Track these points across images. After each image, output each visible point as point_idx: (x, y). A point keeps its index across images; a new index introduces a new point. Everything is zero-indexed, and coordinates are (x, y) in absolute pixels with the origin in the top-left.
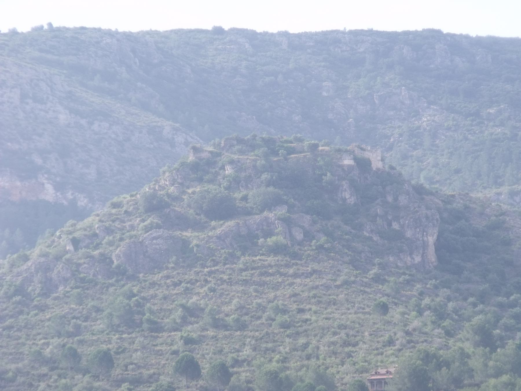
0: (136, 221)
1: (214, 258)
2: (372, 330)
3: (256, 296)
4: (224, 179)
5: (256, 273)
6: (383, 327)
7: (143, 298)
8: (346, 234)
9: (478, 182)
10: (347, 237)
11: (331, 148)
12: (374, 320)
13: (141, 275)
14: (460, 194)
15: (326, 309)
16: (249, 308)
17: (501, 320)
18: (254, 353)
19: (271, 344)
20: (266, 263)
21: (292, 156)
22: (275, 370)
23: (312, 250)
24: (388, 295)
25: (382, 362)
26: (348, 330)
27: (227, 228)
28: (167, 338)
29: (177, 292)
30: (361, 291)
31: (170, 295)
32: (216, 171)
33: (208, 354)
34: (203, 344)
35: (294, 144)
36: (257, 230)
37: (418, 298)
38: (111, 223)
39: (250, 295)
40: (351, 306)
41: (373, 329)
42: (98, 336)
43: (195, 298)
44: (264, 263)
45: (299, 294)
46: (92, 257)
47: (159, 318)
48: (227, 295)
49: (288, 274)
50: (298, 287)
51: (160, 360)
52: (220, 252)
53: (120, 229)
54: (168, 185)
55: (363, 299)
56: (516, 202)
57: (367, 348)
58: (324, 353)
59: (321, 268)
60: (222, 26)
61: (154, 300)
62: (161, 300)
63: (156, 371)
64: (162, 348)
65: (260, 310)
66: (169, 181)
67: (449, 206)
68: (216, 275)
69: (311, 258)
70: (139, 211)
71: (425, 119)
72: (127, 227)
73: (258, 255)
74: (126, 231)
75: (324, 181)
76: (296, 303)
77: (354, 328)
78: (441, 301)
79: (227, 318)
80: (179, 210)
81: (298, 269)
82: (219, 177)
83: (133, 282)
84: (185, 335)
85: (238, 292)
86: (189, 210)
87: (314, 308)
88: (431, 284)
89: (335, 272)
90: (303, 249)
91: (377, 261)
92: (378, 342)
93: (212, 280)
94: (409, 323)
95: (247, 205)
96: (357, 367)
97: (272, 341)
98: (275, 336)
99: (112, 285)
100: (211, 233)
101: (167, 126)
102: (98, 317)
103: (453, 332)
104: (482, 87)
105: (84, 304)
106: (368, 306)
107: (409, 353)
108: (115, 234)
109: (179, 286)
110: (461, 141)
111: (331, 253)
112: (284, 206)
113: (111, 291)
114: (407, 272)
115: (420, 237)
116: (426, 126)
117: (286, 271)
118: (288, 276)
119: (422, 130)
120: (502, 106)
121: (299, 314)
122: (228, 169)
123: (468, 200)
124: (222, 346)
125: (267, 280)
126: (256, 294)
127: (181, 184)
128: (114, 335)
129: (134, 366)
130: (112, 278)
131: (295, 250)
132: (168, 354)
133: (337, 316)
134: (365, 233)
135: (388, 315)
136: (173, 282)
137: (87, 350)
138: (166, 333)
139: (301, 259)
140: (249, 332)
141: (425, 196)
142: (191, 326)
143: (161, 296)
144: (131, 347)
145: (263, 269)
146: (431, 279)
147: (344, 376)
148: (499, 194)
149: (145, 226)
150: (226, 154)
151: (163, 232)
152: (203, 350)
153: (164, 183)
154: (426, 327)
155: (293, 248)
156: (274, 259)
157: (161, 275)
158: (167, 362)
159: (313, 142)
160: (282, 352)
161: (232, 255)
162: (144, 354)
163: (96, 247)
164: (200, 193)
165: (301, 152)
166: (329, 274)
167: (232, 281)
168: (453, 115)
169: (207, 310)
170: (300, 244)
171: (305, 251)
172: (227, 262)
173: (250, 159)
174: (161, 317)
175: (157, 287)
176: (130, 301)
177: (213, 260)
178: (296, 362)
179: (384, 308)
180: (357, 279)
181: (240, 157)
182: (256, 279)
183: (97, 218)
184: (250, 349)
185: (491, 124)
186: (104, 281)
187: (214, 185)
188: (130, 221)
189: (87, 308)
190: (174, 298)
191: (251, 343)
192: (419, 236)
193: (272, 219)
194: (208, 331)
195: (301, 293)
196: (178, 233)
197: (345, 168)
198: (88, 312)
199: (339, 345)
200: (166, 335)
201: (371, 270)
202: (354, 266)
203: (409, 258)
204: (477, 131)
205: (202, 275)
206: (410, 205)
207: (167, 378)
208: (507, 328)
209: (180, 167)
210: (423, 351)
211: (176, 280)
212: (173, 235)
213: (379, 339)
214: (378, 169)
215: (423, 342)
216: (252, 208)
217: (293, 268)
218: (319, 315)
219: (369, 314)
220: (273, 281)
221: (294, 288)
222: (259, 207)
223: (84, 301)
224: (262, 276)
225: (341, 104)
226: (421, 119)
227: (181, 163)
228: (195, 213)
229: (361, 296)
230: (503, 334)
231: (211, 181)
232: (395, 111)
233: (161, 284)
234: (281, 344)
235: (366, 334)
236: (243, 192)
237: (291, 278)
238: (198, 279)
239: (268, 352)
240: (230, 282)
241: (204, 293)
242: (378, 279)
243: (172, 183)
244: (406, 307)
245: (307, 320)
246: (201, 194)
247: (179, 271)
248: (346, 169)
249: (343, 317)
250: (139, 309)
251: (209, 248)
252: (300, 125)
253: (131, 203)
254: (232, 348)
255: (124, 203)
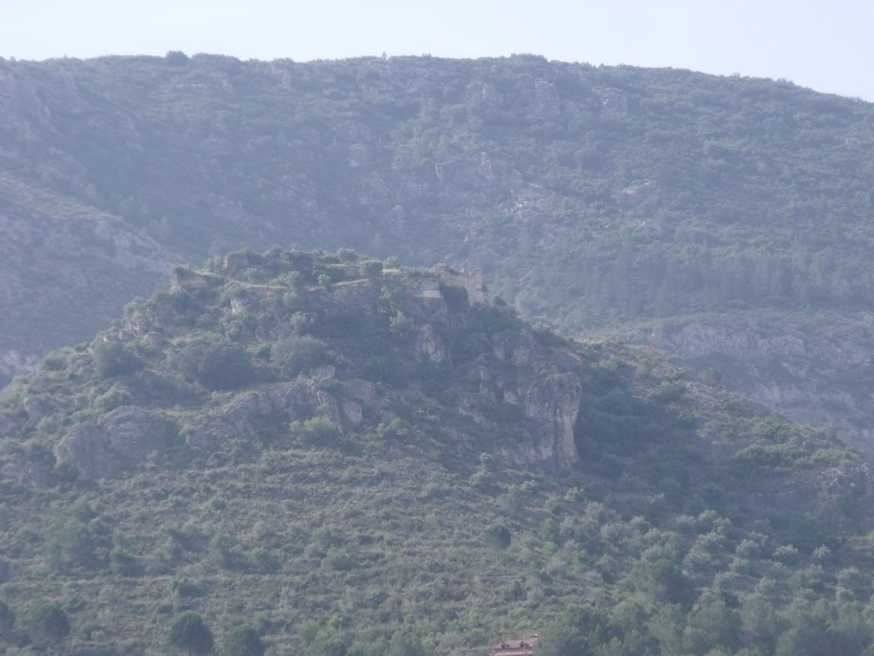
0: (89, 391)
1: (219, 453)
2: (485, 573)
3: (291, 516)
4: (229, 322)
5: (288, 477)
6: (503, 568)
7: (108, 519)
8: (431, 413)
9: (611, 310)
10: (433, 417)
11: (402, 270)
12: (487, 557)
13: (102, 481)
14: (608, 344)
15: (407, 537)
16: (282, 536)
17: (687, 553)
18: (295, 612)
19: (321, 596)
20: (304, 461)
21: (340, 284)
22: (341, 643)
23: (379, 439)
24: (504, 514)
25: (507, 626)
26: (446, 573)
27: (238, 403)
28: (151, 585)
29: (163, 509)
30: (461, 507)
31: (150, 514)
32: (216, 309)
33: (220, 612)
34: (210, 595)
35: (342, 263)
36: (287, 406)
37: (553, 518)
38: (48, 394)
39: (281, 514)
40: (448, 533)
41: (487, 572)
42: (39, 582)
43: (192, 520)
44: (300, 460)
45: (361, 513)
46: (20, 451)
47: (135, 553)
48: (245, 514)
49: (341, 479)
50: (359, 500)
51: (142, 622)
52: (229, 442)
53: (63, 405)
54: (138, 332)
55: (465, 520)
56: (675, 344)
57: (480, 603)
58: (410, 612)
59: (394, 470)
60: (182, 51)
61: (125, 521)
62: (136, 521)
63: (137, 640)
64: (144, 603)
65: (298, 539)
66: (140, 325)
67: (593, 365)
68: (223, 482)
69: (376, 452)
70: (94, 375)
71: (520, 205)
72: (76, 401)
73: (290, 448)
74: (73, 409)
75: (392, 325)
76: (357, 528)
77: (457, 570)
78: (591, 523)
79: (246, 553)
80: (159, 374)
81: (356, 471)
82: (222, 319)
83: (89, 493)
84: (181, 581)
85: (261, 509)
86: (175, 374)
87: (387, 536)
88: (571, 494)
89: (416, 476)
90: (364, 438)
91: (483, 456)
92: (497, 593)
93: (218, 489)
94: (543, 561)
95: (269, 365)
96: (467, 635)
97: (324, 590)
98: (328, 582)
99: (55, 497)
100: (212, 411)
101: (101, 220)
102: (36, 550)
103: (613, 574)
104: (612, 151)
105: (11, 529)
106: (474, 532)
107: (550, 612)
108: (55, 414)
109: (164, 499)
110: (581, 241)
111: (408, 443)
112: (329, 366)
113: (54, 507)
114: (532, 475)
115: (549, 416)
116: (521, 217)
117: (336, 474)
118: (341, 483)
119: (515, 224)
120: (647, 184)
121: (363, 546)
122: (237, 306)
123: (622, 354)
124: (241, 599)
125: (307, 489)
126: (291, 512)
127: (160, 330)
128: (65, 580)
129: (101, 632)
130: (55, 486)
131: (351, 440)
132: (155, 612)
133: (426, 549)
134: (461, 411)
135: (508, 548)
136: (154, 492)
137: (22, 605)
138: (149, 578)
139: (360, 455)
140: (284, 575)
141: (552, 348)
142: (189, 566)
143: (136, 516)
144: (94, 600)
145: (299, 471)
146: (569, 486)
147: (446, 650)
148: (648, 331)
149: (105, 400)
150: (233, 281)
151: (135, 410)
152: (211, 606)
153: (131, 328)
154: (571, 567)
155: (347, 436)
156: (316, 454)
157: (133, 481)
158: (154, 626)
159: (373, 261)
160: (342, 610)
161: (247, 448)
162: (115, 613)
163: (26, 435)
164: (193, 346)
165: (353, 278)
166: (408, 479)
167: (250, 491)
168: (565, 198)
169: (215, 539)
170: (357, 429)
171: (367, 441)
172: (239, 459)
173: (272, 290)
174: (139, 551)
175: (129, 501)
176: (87, 525)
177: (217, 456)
178: (366, 626)
179: (503, 537)
180: (453, 488)
181: (255, 286)
182: (289, 487)
183: (25, 387)
184: (288, 604)
185: (630, 213)
186: (41, 491)
187: (214, 332)
188: (80, 391)
189: (17, 535)
190: (158, 519)
191: (290, 593)
192: (548, 416)
193: (311, 389)
194: (216, 574)
195: (364, 511)
196: (159, 412)
197: (425, 303)
198: (19, 542)
199: (434, 598)
200: (149, 581)
201: (476, 471)
202: (446, 466)
203: (533, 451)
204: (606, 224)
205: (201, 481)
206: (533, 365)
207: (157, 652)
208: (699, 567)
209: (158, 301)
210: (578, 610)
211: (159, 490)
212: (151, 415)
213: (498, 588)
214: (478, 304)
215: (569, 593)
216: (278, 370)
217: (348, 470)
218: (396, 547)
219: (478, 545)
220: (316, 491)
221: (351, 503)
222: (290, 369)
223: (12, 524)
224: (298, 483)
225: (381, 181)
226: (513, 205)
227: (159, 296)
228: (185, 378)
229: (462, 516)
230: (693, 576)
231: (208, 326)
232: (469, 192)
233: (135, 495)
234: (339, 595)
235: (477, 579)
236: (260, 343)
237: (345, 486)
238: (195, 487)
239: (317, 609)
240: (247, 493)
241: (205, 511)
242: (487, 488)
243: (145, 328)
244: (535, 532)
245: (377, 556)
246: (194, 348)
247: (163, 475)
248: (428, 306)
249: (436, 550)
250: (102, 537)
251: (210, 436)
252: (315, 215)
253: (79, 361)
254: (259, 602)
255: (68, 361)
